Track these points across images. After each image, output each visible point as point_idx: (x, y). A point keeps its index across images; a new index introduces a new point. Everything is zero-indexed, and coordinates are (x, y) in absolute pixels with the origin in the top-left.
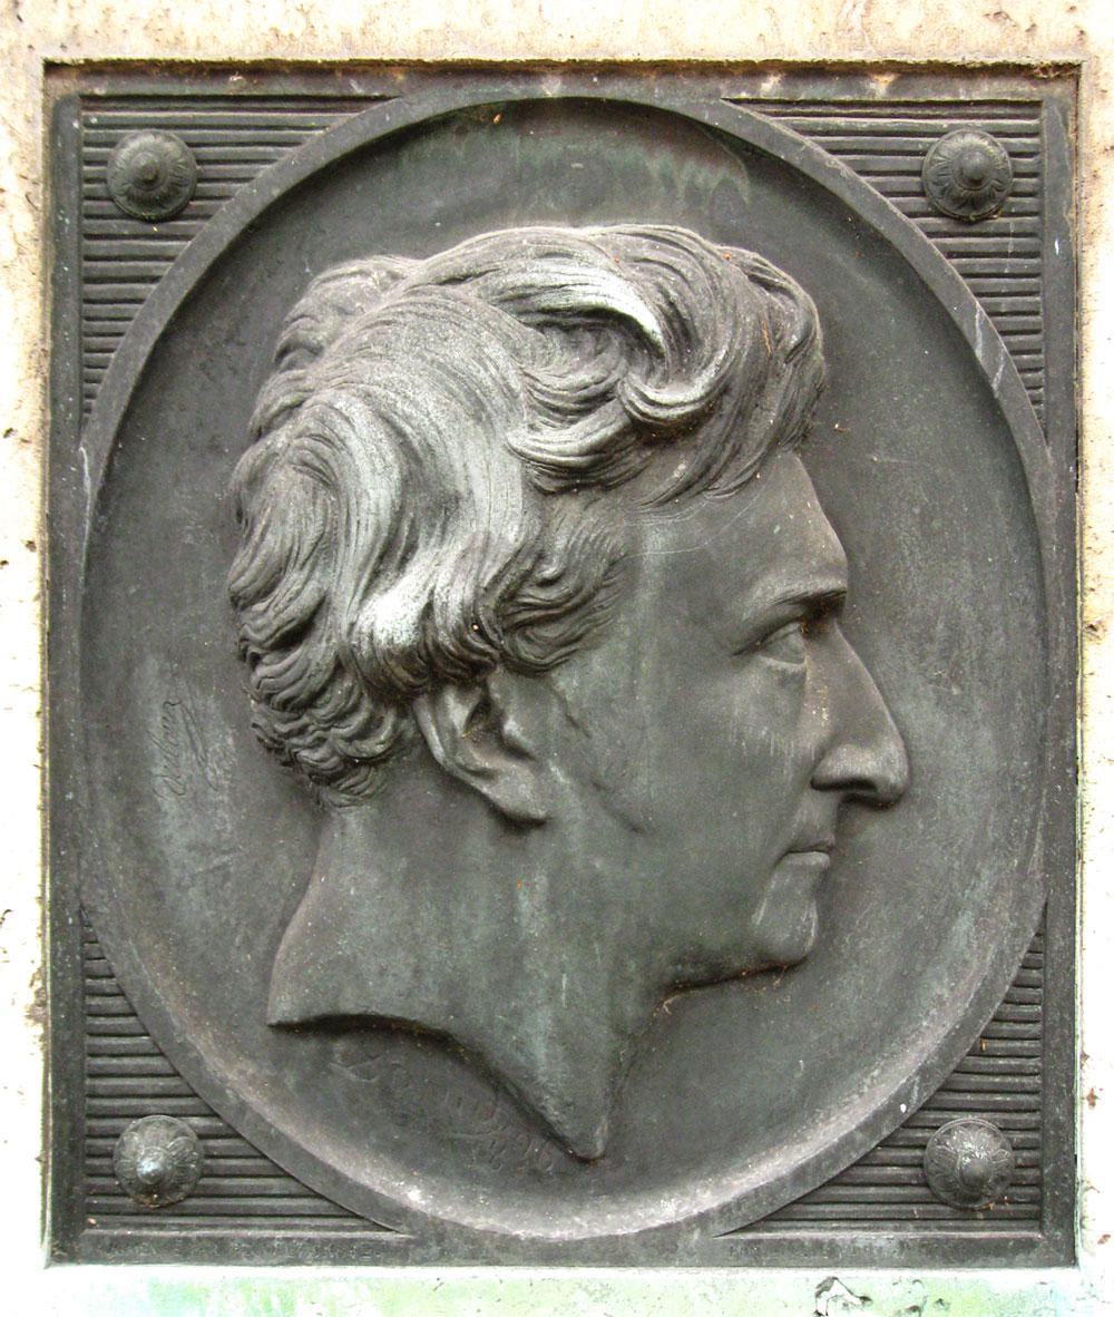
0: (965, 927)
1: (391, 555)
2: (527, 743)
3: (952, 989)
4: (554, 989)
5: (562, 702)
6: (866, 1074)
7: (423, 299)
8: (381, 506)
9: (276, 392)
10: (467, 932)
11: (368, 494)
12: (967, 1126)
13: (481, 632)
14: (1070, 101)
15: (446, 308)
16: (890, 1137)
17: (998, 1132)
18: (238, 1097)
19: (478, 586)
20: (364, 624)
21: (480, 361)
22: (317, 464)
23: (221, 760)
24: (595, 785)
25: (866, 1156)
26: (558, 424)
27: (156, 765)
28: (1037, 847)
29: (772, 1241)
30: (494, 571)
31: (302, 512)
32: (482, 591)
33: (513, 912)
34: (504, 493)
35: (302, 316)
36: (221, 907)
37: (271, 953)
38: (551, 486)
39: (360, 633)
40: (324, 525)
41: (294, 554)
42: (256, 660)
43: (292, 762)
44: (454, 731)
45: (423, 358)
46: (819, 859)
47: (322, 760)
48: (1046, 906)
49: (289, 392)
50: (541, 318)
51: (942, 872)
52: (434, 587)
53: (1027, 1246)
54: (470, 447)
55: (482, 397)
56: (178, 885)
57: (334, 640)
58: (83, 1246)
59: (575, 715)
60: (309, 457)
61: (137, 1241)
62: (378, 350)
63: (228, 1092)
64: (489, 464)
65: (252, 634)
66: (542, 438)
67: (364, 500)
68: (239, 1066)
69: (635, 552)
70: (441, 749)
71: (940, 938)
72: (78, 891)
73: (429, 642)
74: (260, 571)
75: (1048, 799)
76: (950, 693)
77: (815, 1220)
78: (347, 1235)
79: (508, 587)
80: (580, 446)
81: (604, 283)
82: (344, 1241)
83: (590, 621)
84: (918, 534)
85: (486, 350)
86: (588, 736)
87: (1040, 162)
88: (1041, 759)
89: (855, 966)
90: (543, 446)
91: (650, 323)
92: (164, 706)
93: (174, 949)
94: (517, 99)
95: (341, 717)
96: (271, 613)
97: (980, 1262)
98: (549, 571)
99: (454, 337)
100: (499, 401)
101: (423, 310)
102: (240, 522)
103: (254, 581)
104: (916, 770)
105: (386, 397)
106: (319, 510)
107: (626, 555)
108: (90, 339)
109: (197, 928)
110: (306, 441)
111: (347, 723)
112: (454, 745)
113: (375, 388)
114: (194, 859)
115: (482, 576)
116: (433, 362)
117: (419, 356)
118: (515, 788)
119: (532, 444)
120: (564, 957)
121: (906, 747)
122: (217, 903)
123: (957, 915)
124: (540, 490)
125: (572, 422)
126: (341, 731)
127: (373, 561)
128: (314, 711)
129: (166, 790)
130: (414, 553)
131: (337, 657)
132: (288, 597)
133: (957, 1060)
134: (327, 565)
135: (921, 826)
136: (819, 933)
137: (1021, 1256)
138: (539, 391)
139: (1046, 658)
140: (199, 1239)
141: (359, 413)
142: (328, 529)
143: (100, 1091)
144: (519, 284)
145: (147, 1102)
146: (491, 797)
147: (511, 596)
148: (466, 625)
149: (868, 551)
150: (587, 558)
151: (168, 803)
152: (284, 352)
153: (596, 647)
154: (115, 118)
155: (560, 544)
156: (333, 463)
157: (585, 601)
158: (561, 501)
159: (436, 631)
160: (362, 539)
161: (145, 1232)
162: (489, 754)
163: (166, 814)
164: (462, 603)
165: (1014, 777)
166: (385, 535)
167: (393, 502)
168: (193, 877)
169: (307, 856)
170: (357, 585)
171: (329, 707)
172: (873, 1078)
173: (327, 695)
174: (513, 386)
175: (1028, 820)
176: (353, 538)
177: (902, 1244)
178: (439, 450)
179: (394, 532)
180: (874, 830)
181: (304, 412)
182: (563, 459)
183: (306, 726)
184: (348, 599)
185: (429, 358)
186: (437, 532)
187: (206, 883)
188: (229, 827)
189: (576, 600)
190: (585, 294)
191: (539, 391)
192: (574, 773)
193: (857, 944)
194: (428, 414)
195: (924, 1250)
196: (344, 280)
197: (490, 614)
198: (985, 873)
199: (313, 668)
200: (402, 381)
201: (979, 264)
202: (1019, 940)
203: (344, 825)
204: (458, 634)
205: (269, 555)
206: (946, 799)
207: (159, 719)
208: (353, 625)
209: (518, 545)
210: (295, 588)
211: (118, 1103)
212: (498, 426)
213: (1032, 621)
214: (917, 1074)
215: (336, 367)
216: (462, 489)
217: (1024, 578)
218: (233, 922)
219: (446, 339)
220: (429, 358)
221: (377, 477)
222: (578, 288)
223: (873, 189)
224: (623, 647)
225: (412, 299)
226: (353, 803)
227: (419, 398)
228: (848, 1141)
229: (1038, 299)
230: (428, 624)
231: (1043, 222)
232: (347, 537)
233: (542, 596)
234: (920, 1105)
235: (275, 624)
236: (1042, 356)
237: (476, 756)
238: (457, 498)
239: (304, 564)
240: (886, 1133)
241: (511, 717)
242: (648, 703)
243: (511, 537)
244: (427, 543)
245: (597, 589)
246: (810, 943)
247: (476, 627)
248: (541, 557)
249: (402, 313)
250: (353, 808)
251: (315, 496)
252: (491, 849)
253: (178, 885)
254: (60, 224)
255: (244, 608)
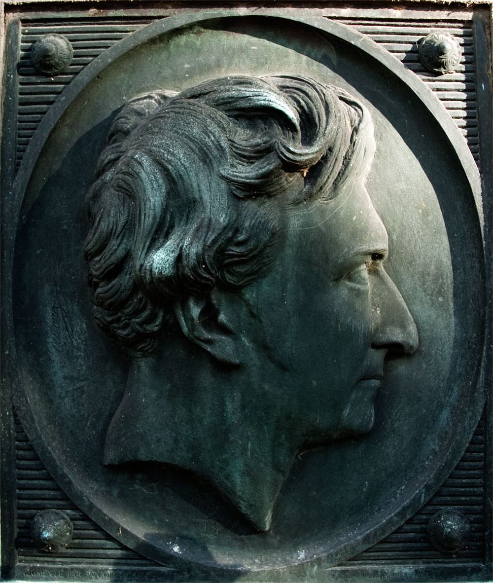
0: (446, 416)
1: (160, 233)
2: (230, 326)
3: (440, 446)
4: (245, 449)
5: (248, 305)
6: (398, 489)
7: (178, 105)
8: (156, 205)
9: (108, 155)
10: (201, 421)
11: (150, 200)
12: (448, 513)
13: (206, 269)
14: (486, 20)
15: (189, 109)
16: (411, 519)
17: (463, 515)
18: (89, 501)
19: (205, 245)
20: (147, 265)
21: (206, 133)
22: (125, 186)
23: (80, 335)
24: (264, 347)
25: (400, 528)
26: (245, 164)
27: (49, 337)
28: (481, 376)
29: (353, 571)
30: (213, 237)
31: (118, 210)
32: (207, 248)
33: (223, 411)
34: (218, 197)
35: (120, 118)
36: (80, 407)
37: (105, 430)
38: (240, 194)
39: (145, 269)
40: (128, 216)
41: (114, 231)
42: (96, 286)
43: (115, 336)
44: (192, 319)
45: (178, 133)
46: (375, 383)
47: (128, 335)
48: (486, 404)
49: (113, 153)
50: (236, 113)
51: (434, 389)
52: (183, 246)
53: (476, 570)
54: (201, 176)
55: (207, 151)
56: (60, 396)
57: (133, 274)
58: (17, 572)
59: (255, 311)
60: (122, 183)
61: (41, 570)
62: (156, 130)
63: (84, 498)
64: (210, 183)
65: (95, 273)
66: (237, 171)
67: (148, 203)
68: (90, 485)
69: (284, 228)
70: (187, 329)
71: (434, 421)
72: (11, 398)
73: (180, 273)
74: (97, 241)
75: (486, 352)
76: (438, 300)
77: (375, 560)
78: (144, 568)
79: (220, 246)
80: (257, 174)
81: (268, 95)
82: (143, 571)
83: (261, 263)
84: (421, 222)
85: (209, 128)
86: (261, 322)
87: (473, 48)
88: (483, 332)
89: (393, 435)
90: (237, 174)
91: (292, 114)
92: (53, 309)
93: (58, 427)
94: (225, 16)
95: (136, 313)
96: (103, 261)
97: (454, 579)
98: (241, 238)
99: (193, 123)
100: (215, 152)
101: (178, 110)
102: (89, 218)
103: (94, 246)
104: (422, 338)
105: (159, 152)
106: (126, 209)
107: (279, 230)
108: (20, 131)
109: (69, 417)
110: (120, 176)
111: (140, 316)
112: (192, 328)
113: (154, 148)
114: (67, 383)
115: (207, 240)
116: (183, 134)
117: (176, 132)
118: (224, 348)
119: (232, 173)
120: (249, 433)
121: (417, 327)
122: (79, 405)
123: (442, 409)
124: (235, 196)
125: (252, 163)
126: (137, 320)
127: (152, 233)
128: (124, 311)
129: (53, 350)
130: (172, 229)
131: (134, 282)
132: (110, 253)
133: (443, 481)
134: (130, 236)
135: (425, 366)
136: (375, 420)
137: (474, 575)
138: (236, 148)
139: (484, 283)
140: (72, 569)
141: (146, 161)
142: (130, 219)
143: (24, 496)
144: (226, 97)
145: (46, 502)
146: (212, 353)
147: (221, 251)
148: (199, 264)
149: (398, 230)
150: (260, 231)
151: (55, 357)
152: (112, 135)
153: (265, 276)
154: (36, 29)
155: (247, 224)
156: (133, 186)
157: (261, 252)
158: (247, 203)
159: (184, 268)
160: (147, 221)
161: (46, 565)
162: (210, 331)
163: (54, 361)
164: (196, 254)
165: (469, 342)
166: (158, 220)
167: (162, 203)
168: (67, 392)
169: (122, 382)
170: (144, 246)
171: (130, 308)
172: (401, 490)
173: (130, 302)
174: (223, 145)
175: (476, 362)
176: (142, 222)
177: (416, 571)
178: (186, 177)
179: (163, 218)
180: (402, 368)
181: (120, 164)
182: (248, 181)
183: (120, 317)
184: (140, 253)
185: (181, 132)
186: (184, 218)
187: (73, 396)
188: (84, 368)
189: (255, 252)
190: (258, 100)
191: (236, 148)
192: (254, 341)
193: (394, 425)
194: (180, 160)
195: (427, 574)
196: (141, 102)
197: (211, 259)
198: (456, 388)
199: (123, 288)
200: (167, 144)
201: (447, 95)
202: (473, 422)
203: (139, 367)
204: (194, 269)
205: (102, 232)
206: (436, 353)
207: (50, 314)
208: (142, 266)
209: (225, 224)
210: (114, 248)
211: (32, 502)
212: (215, 165)
213: (477, 265)
214: (424, 488)
215: (136, 140)
216: (197, 196)
217: (472, 244)
218: (86, 415)
219: (189, 124)
220: (181, 132)
221: (155, 191)
222: (255, 98)
223: (396, 59)
224: (278, 277)
225: (173, 106)
226: (144, 356)
227: (176, 152)
228: (390, 522)
229: (475, 111)
230: (180, 265)
231: (476, 76)
232: (139, 222)
233: (238, 250)
234: (425, 503)
235: (104, 266)
236: (478, 138)
237: (204, 332)
238: (195, 201)
239: (118, 236)
240: (408, 517)
241: (222, 313)
242: (291, 305)
243: (222, 220)
244: (179, 224)
245: (265, 247)
246: (371, 424)
247: (204, 266)
248: (237, 231)
249: (168, 112)
250: (144, 358)
251: (124, 202)
252: (212, 379)
253: (60, 396)
254: (9, 78)
255: (91, 260)
